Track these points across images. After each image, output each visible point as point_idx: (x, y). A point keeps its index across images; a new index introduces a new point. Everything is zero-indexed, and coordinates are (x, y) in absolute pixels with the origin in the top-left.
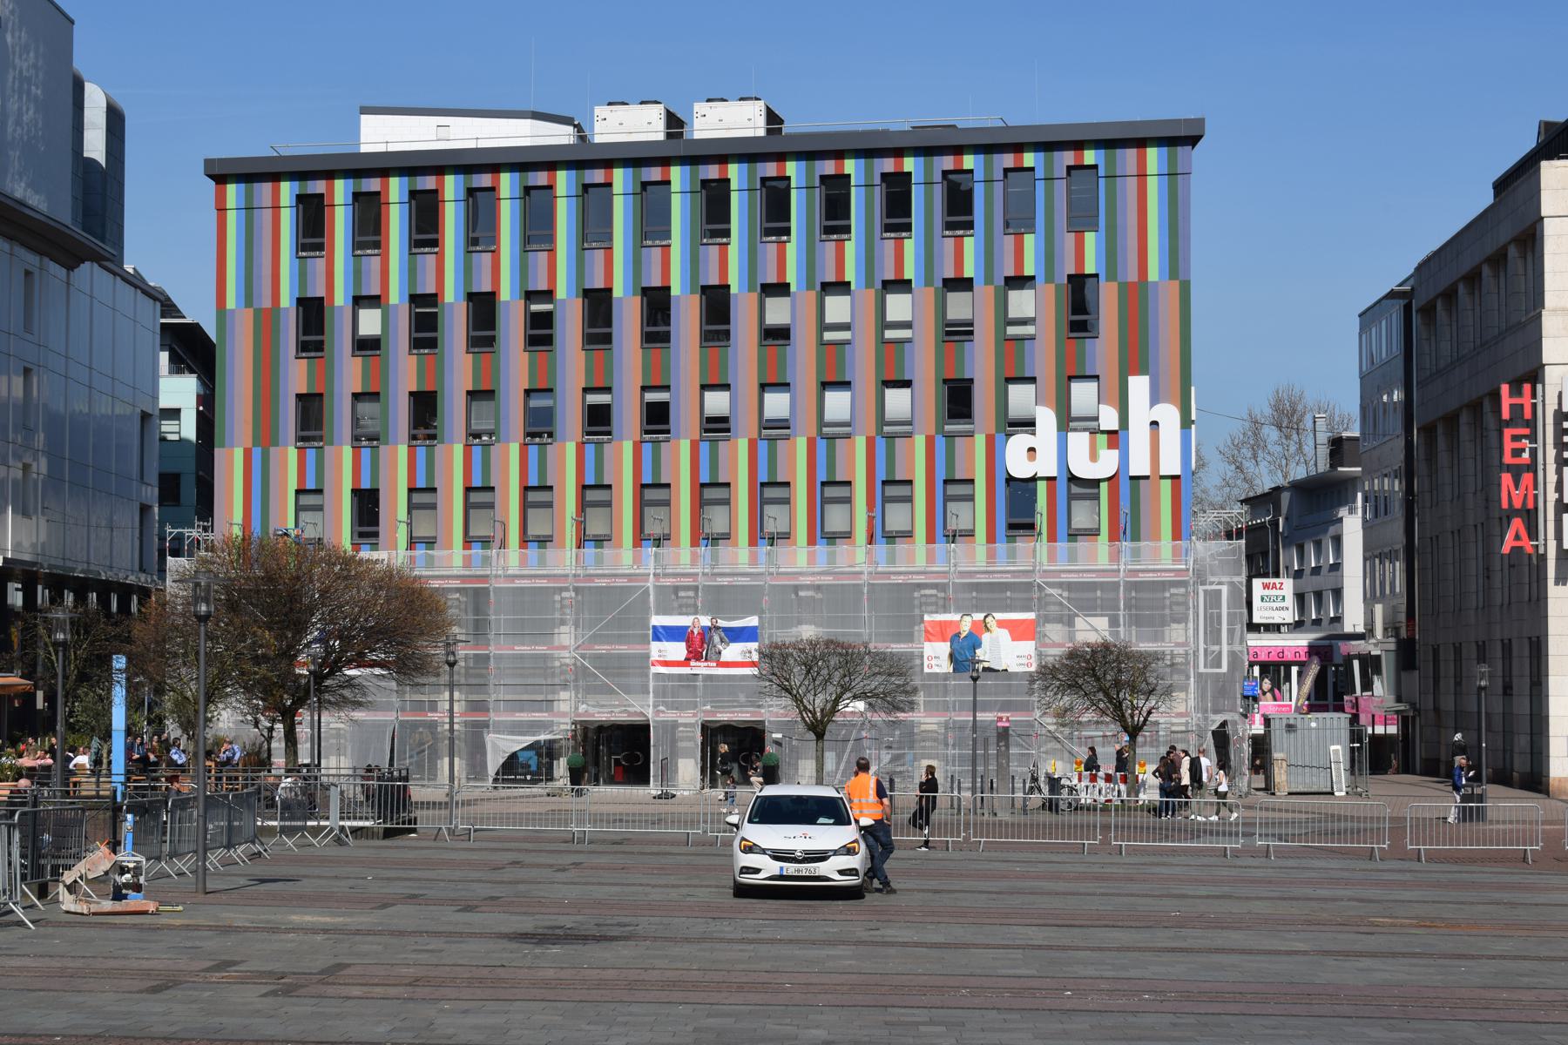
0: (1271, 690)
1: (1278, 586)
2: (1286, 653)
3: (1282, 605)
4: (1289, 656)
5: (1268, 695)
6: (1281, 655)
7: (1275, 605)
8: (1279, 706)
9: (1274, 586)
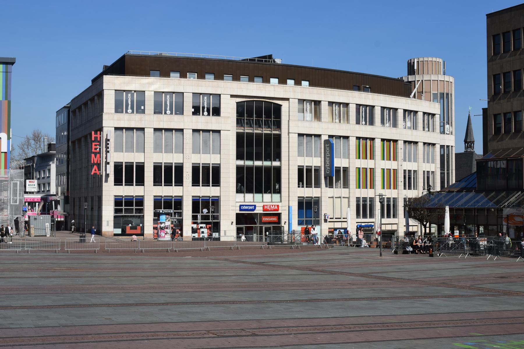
0: (31, 209)
1: (33, 182)
2: (35, 199)
3: (34, 187)
4: (36, 200)
5: (30, 210)
6: (33, 200)
7: (32, 187)
8: (33, 213)
9: (32, 182)
